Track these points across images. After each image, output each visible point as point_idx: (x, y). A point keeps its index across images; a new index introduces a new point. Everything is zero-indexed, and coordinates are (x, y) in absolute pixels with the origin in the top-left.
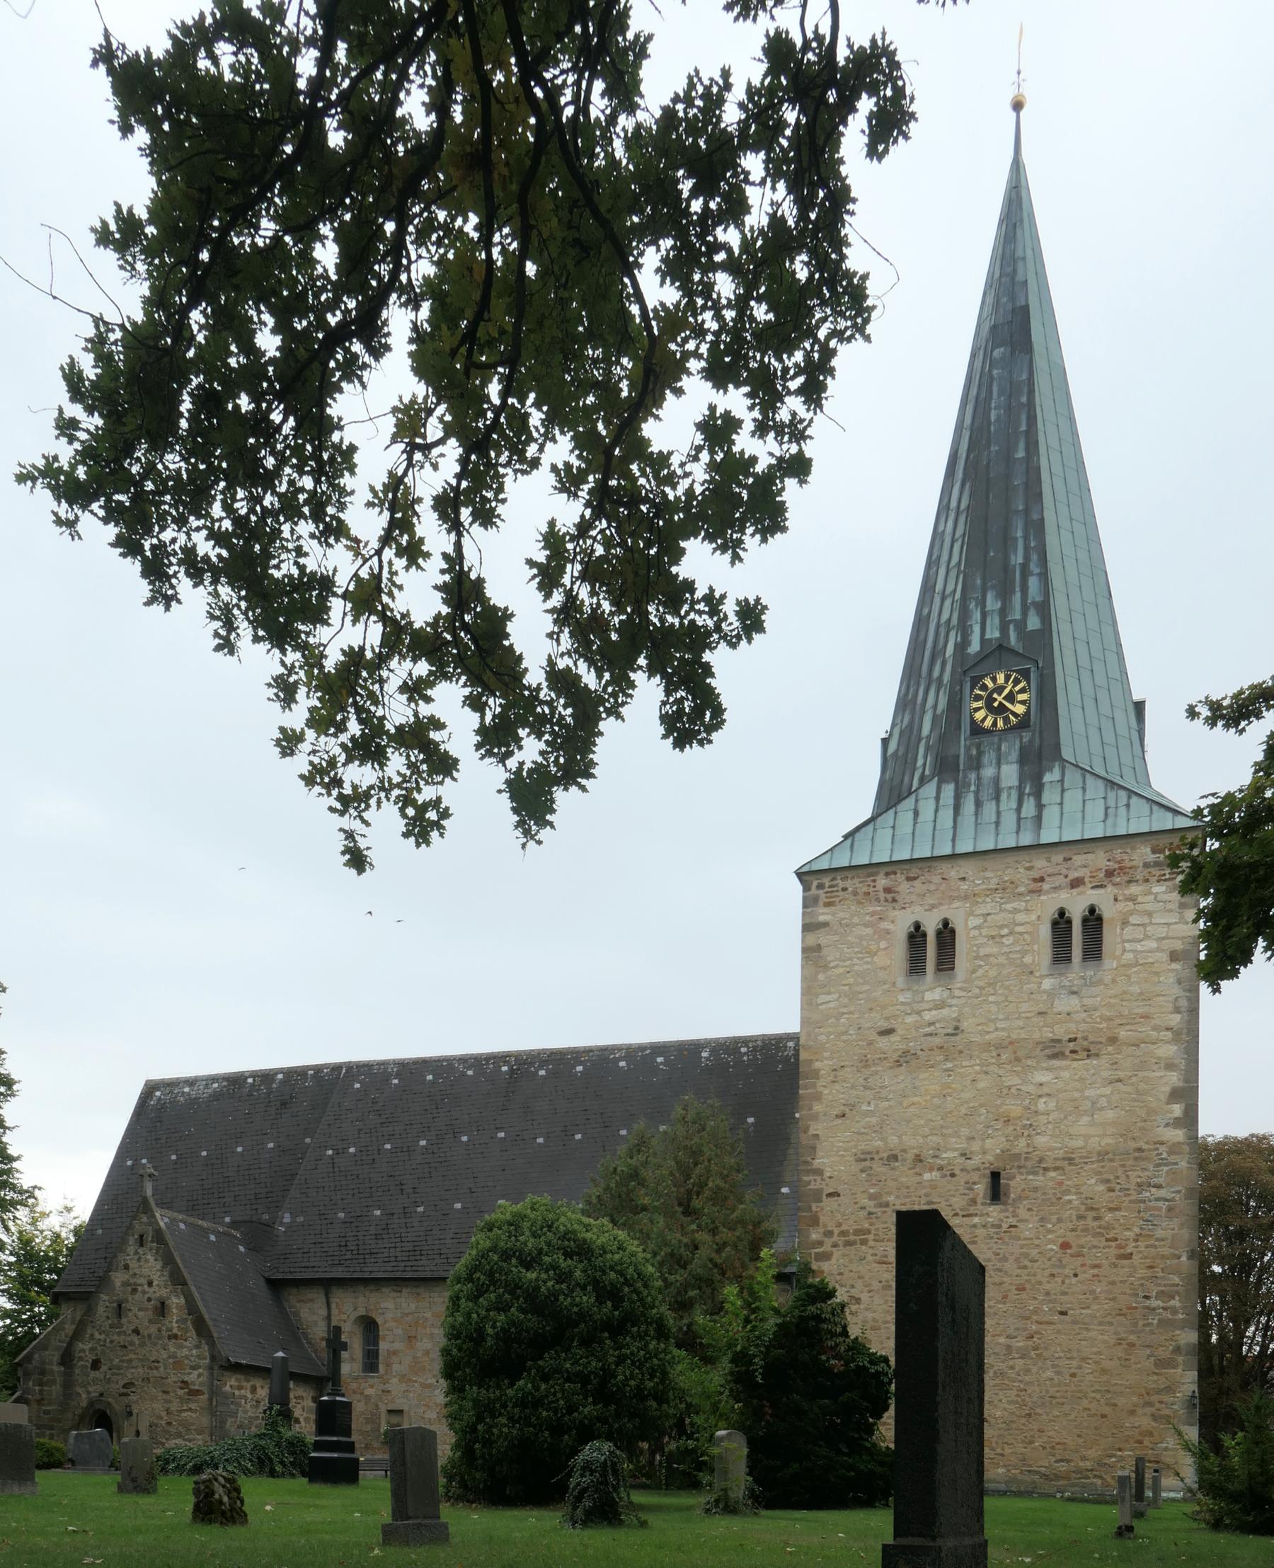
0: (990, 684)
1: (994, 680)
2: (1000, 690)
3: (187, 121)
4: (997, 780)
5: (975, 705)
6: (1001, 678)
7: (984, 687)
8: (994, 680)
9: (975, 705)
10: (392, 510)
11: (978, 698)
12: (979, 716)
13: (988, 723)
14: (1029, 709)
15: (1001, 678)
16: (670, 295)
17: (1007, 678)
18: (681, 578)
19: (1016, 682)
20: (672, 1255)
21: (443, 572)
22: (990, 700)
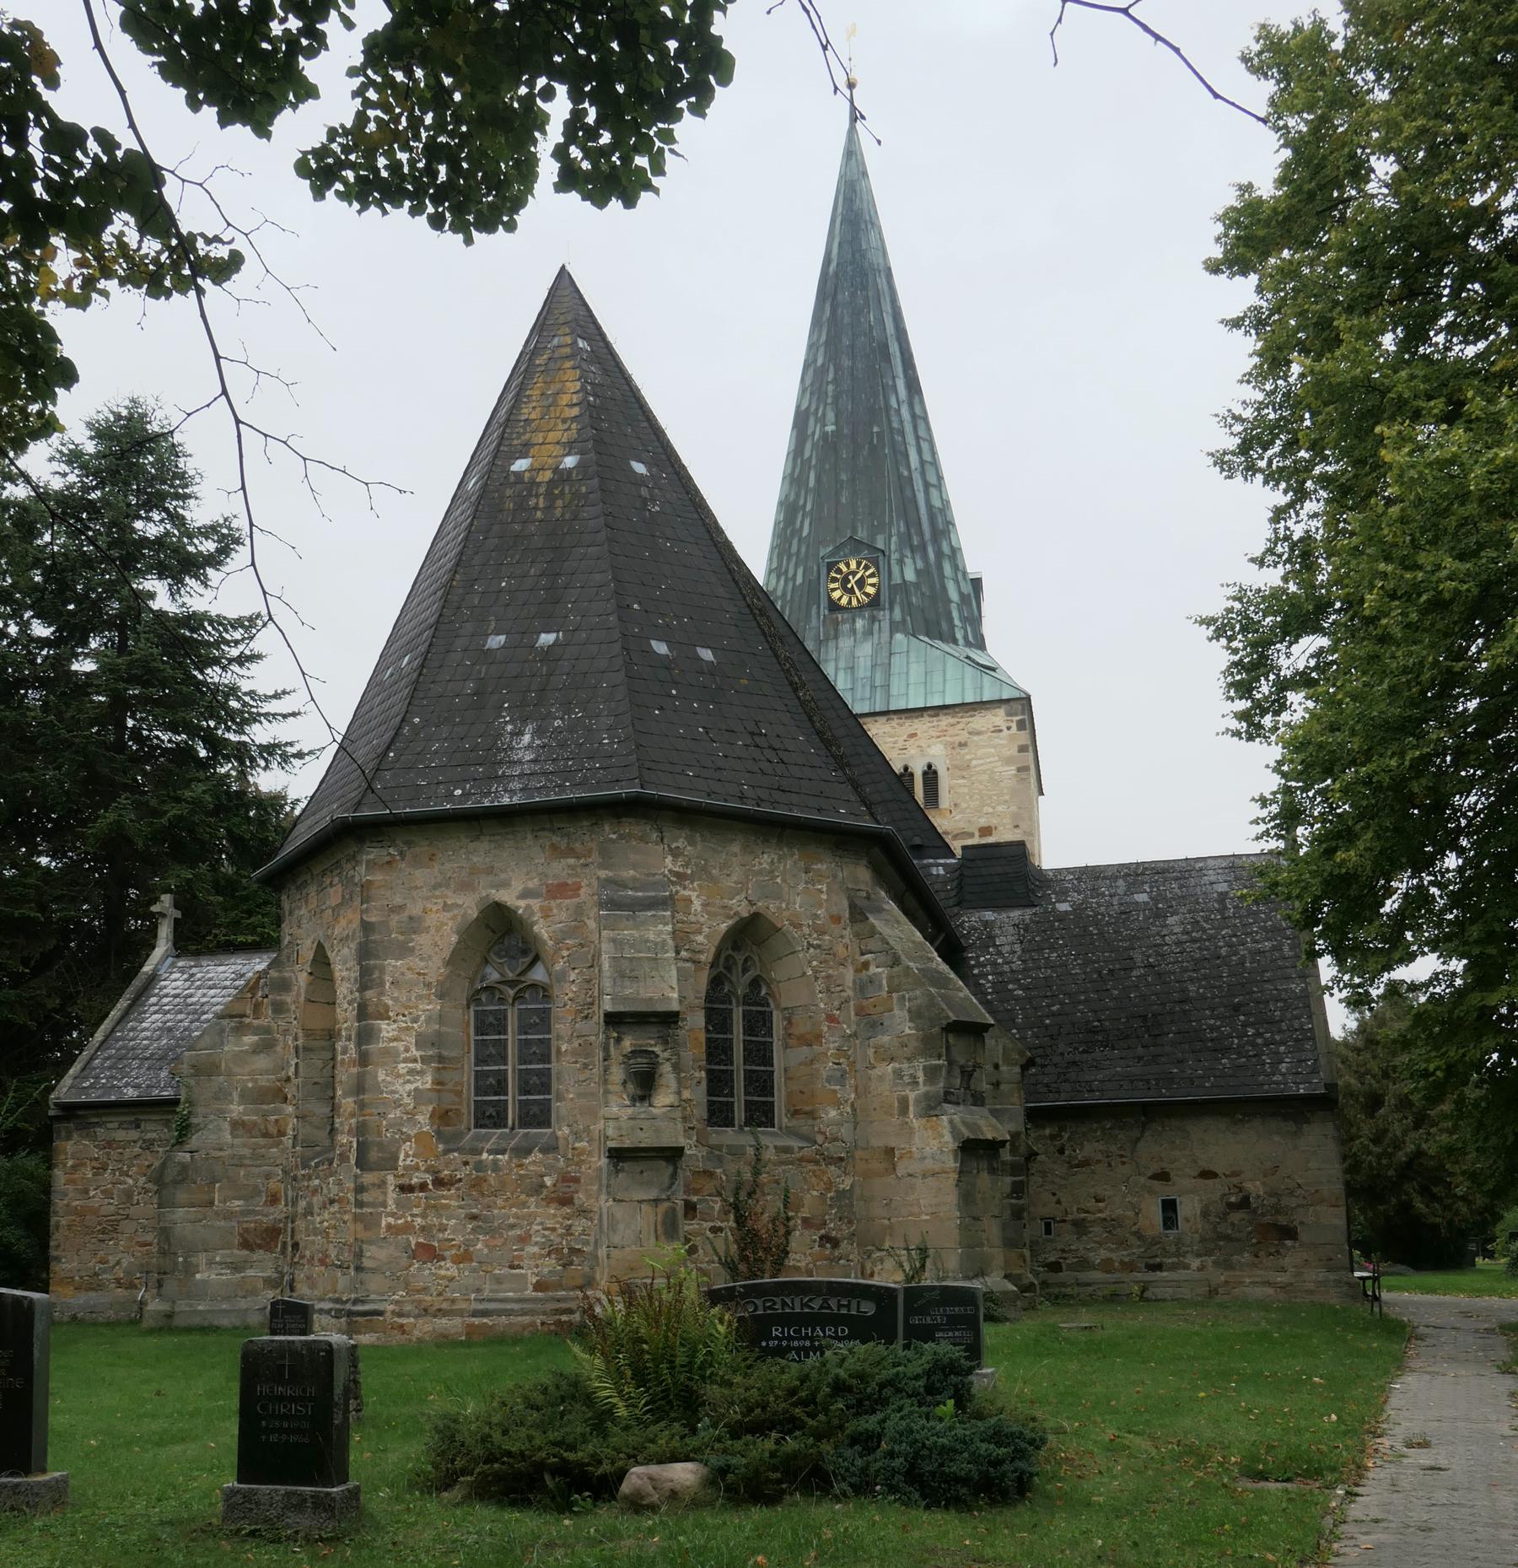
0: (844, 569)
1: (848, 565)
2: (854, 573)
3: (449, 92)
4: (853, 656)
5: (832, 586)
6: (853, 565)
7: (839, 571)
8: (848, 565)
9: (832, 586)
10: (1316, 668)
11: (834, 580)
12: (836, 595)
13: (844, 601)
14: (878, 591)
15: (853, 565)
16: (1294, 698)
17: (859, 564)
18: (144, 290)
19: (866, 568)
20: (1023, 1473)
21: (105, 294)
22: (846, 580)
